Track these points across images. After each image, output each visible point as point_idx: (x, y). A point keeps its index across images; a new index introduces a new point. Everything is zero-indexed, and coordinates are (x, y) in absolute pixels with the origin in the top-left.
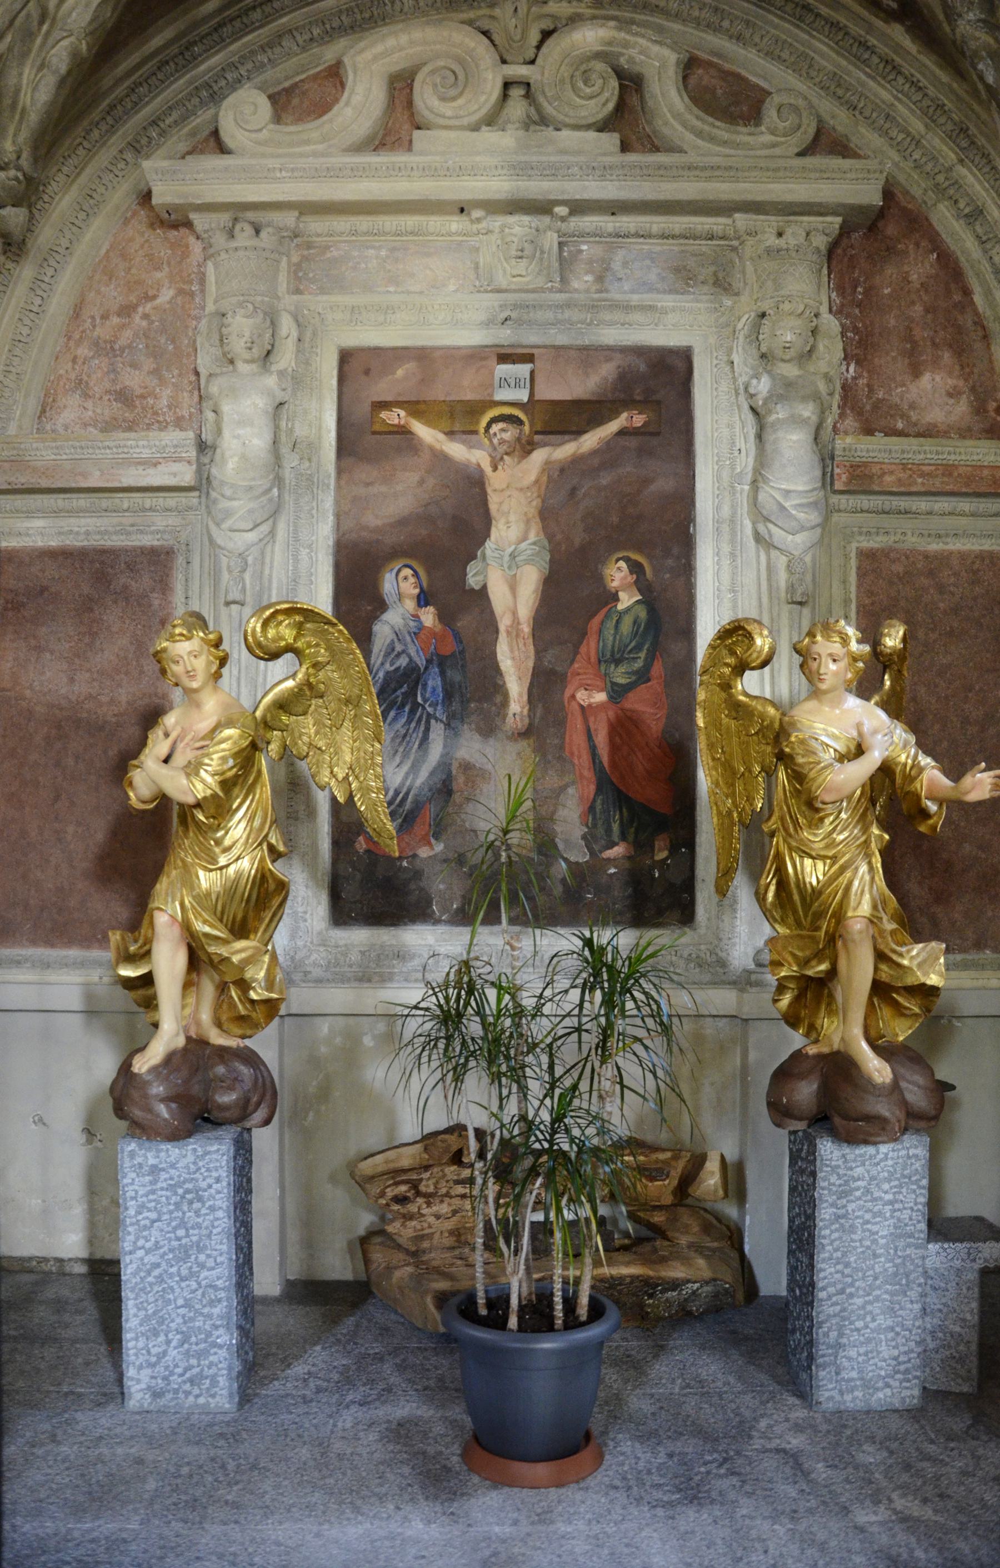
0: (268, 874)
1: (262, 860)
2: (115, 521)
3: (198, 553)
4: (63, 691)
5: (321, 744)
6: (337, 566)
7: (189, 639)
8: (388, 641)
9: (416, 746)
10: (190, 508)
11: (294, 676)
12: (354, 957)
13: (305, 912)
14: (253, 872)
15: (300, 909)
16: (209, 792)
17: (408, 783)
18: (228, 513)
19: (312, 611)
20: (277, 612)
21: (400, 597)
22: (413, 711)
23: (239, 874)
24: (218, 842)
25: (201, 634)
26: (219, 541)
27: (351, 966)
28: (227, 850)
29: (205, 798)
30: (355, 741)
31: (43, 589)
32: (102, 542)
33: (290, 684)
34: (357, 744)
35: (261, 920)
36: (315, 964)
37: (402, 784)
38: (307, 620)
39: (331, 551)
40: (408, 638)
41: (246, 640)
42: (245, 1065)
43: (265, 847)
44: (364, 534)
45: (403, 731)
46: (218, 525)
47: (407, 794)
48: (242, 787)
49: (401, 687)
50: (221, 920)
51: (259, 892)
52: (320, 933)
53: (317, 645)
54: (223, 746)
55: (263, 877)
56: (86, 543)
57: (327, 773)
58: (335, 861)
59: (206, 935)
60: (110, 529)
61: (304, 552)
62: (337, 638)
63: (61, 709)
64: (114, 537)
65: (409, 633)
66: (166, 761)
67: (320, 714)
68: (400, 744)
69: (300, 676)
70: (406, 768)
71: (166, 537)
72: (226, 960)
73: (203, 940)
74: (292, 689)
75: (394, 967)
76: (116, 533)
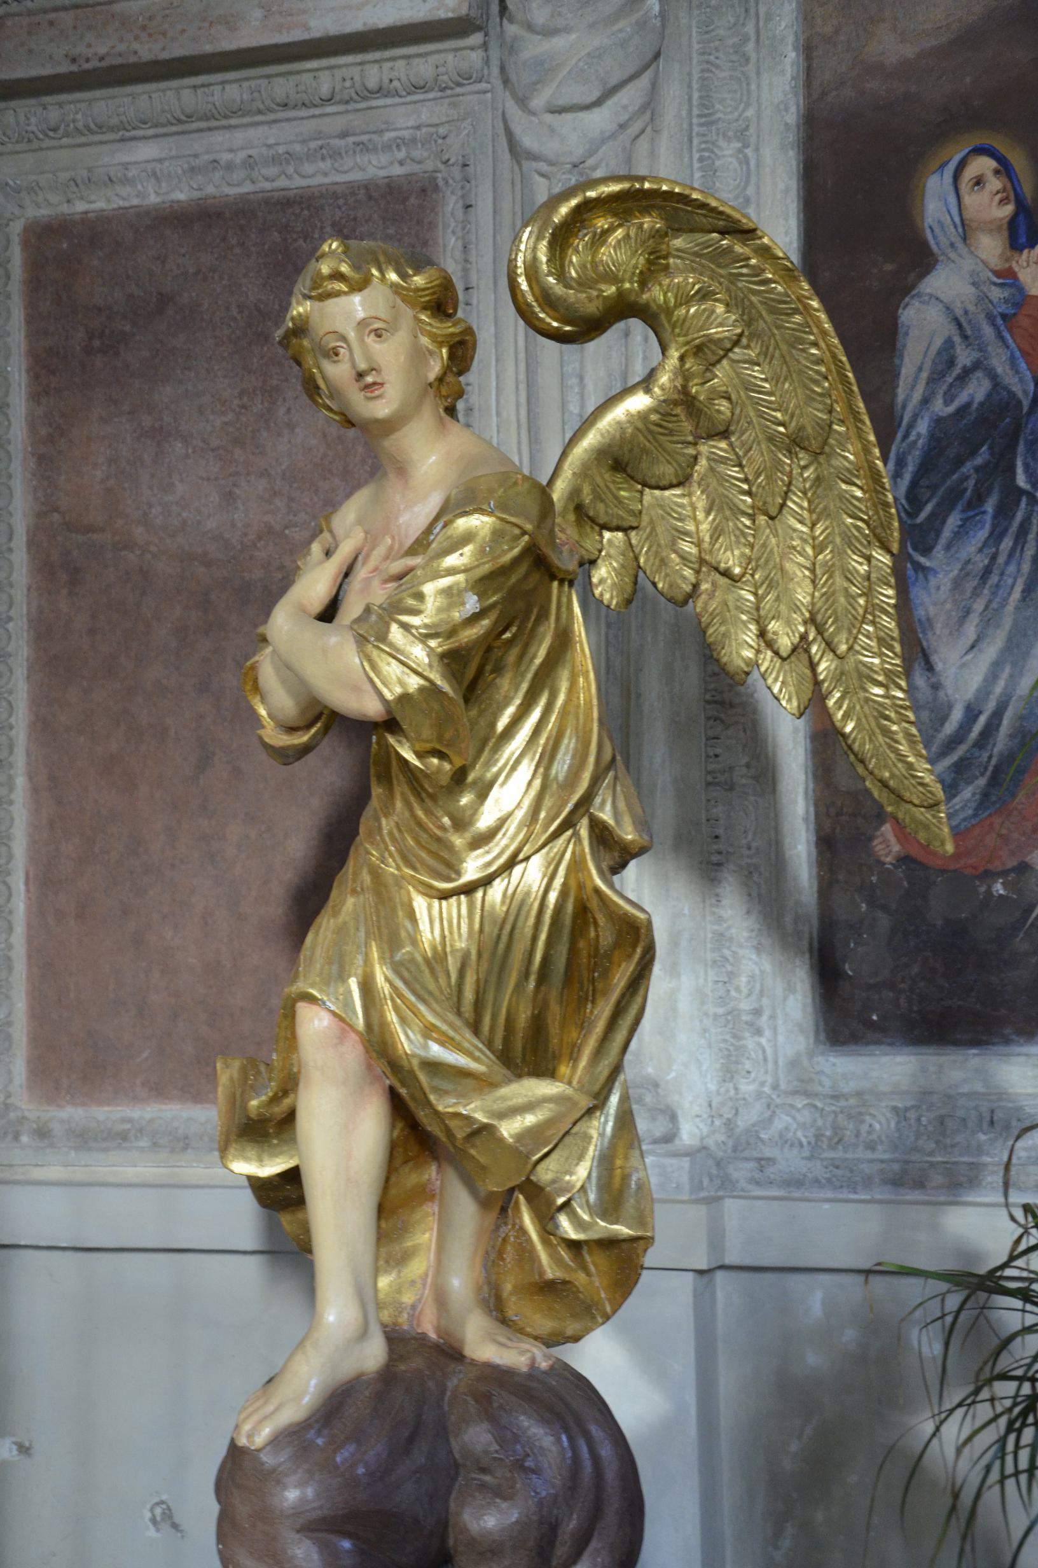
0: (594, 904)
1: (577, 864)
2: (309, 127)
3: (488, 185)
4: (211, 524)
5: (732, 560)
6: (810, 174)
7: (360, 285)
8: (938, 343)
9: (1016, 594)
10: (465, 77)
11: (646, 383)
12: (880, 1122)
13: (757, 1012)
14: (553, 897)
15: (745, 1005)
16: (414, 683)
17: (998, 689)
18: (545, 69)
19: (684, 199)
20: (587, 207)
21: (966, 230)
22: (1004, 512)
23: (517, 904)
24: (461, 823)
25: (393, 276)
26: (528, 141)
27: (870, 1146)
28: (482, 840)
29: (404, 698)
30: (819, 549)
31: (164, 301)
32: (282, 183)
33: (639, 402)
34: (826, 556)
35: (584, 1026)
36: (783, 1140)
37: (984, 692)
38: (676, 226)
39: (791, 137)
40: (988, 331)
41: (513, 286)
42: (543, 1421)
43: (584, 832)
44: (871, 85)
45: (982, 561)
46: (522, 102)
47: (998, 714)
48: (519, 675)
49: (973, 453)
50: (476, 1028)
51: (573, 951)
52: (794, 1064)
53: (704, 295)
54: (452, 560)
55: (583, 912)
56: (247, 188)
57: (750, 635)
58: (826, 889)
59: (434, 1067)
60: (298, 148)
61: (728, 150)
62: (758, 271)
63: (208, 564)
64: (309, 168)
65: (990, 318)
66: (328, 614)
67: (723, 479)
68: (976, 593)
69: (664, 379)
70: (991, 651)
71: (417, 153)
72: (484, 1131)
73: (422, 1077)
74: (643, 416)
75: (980, 1150)
76: (310, 157)
